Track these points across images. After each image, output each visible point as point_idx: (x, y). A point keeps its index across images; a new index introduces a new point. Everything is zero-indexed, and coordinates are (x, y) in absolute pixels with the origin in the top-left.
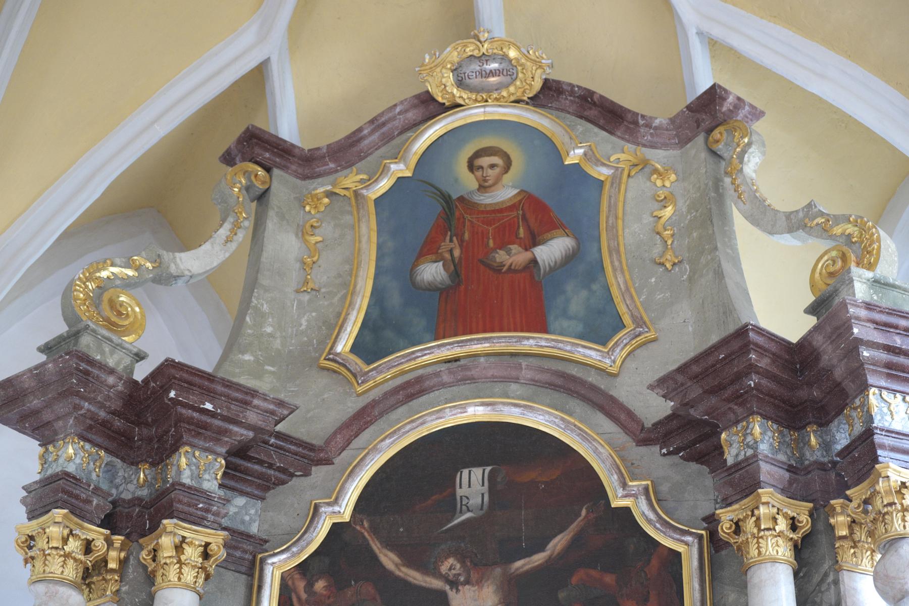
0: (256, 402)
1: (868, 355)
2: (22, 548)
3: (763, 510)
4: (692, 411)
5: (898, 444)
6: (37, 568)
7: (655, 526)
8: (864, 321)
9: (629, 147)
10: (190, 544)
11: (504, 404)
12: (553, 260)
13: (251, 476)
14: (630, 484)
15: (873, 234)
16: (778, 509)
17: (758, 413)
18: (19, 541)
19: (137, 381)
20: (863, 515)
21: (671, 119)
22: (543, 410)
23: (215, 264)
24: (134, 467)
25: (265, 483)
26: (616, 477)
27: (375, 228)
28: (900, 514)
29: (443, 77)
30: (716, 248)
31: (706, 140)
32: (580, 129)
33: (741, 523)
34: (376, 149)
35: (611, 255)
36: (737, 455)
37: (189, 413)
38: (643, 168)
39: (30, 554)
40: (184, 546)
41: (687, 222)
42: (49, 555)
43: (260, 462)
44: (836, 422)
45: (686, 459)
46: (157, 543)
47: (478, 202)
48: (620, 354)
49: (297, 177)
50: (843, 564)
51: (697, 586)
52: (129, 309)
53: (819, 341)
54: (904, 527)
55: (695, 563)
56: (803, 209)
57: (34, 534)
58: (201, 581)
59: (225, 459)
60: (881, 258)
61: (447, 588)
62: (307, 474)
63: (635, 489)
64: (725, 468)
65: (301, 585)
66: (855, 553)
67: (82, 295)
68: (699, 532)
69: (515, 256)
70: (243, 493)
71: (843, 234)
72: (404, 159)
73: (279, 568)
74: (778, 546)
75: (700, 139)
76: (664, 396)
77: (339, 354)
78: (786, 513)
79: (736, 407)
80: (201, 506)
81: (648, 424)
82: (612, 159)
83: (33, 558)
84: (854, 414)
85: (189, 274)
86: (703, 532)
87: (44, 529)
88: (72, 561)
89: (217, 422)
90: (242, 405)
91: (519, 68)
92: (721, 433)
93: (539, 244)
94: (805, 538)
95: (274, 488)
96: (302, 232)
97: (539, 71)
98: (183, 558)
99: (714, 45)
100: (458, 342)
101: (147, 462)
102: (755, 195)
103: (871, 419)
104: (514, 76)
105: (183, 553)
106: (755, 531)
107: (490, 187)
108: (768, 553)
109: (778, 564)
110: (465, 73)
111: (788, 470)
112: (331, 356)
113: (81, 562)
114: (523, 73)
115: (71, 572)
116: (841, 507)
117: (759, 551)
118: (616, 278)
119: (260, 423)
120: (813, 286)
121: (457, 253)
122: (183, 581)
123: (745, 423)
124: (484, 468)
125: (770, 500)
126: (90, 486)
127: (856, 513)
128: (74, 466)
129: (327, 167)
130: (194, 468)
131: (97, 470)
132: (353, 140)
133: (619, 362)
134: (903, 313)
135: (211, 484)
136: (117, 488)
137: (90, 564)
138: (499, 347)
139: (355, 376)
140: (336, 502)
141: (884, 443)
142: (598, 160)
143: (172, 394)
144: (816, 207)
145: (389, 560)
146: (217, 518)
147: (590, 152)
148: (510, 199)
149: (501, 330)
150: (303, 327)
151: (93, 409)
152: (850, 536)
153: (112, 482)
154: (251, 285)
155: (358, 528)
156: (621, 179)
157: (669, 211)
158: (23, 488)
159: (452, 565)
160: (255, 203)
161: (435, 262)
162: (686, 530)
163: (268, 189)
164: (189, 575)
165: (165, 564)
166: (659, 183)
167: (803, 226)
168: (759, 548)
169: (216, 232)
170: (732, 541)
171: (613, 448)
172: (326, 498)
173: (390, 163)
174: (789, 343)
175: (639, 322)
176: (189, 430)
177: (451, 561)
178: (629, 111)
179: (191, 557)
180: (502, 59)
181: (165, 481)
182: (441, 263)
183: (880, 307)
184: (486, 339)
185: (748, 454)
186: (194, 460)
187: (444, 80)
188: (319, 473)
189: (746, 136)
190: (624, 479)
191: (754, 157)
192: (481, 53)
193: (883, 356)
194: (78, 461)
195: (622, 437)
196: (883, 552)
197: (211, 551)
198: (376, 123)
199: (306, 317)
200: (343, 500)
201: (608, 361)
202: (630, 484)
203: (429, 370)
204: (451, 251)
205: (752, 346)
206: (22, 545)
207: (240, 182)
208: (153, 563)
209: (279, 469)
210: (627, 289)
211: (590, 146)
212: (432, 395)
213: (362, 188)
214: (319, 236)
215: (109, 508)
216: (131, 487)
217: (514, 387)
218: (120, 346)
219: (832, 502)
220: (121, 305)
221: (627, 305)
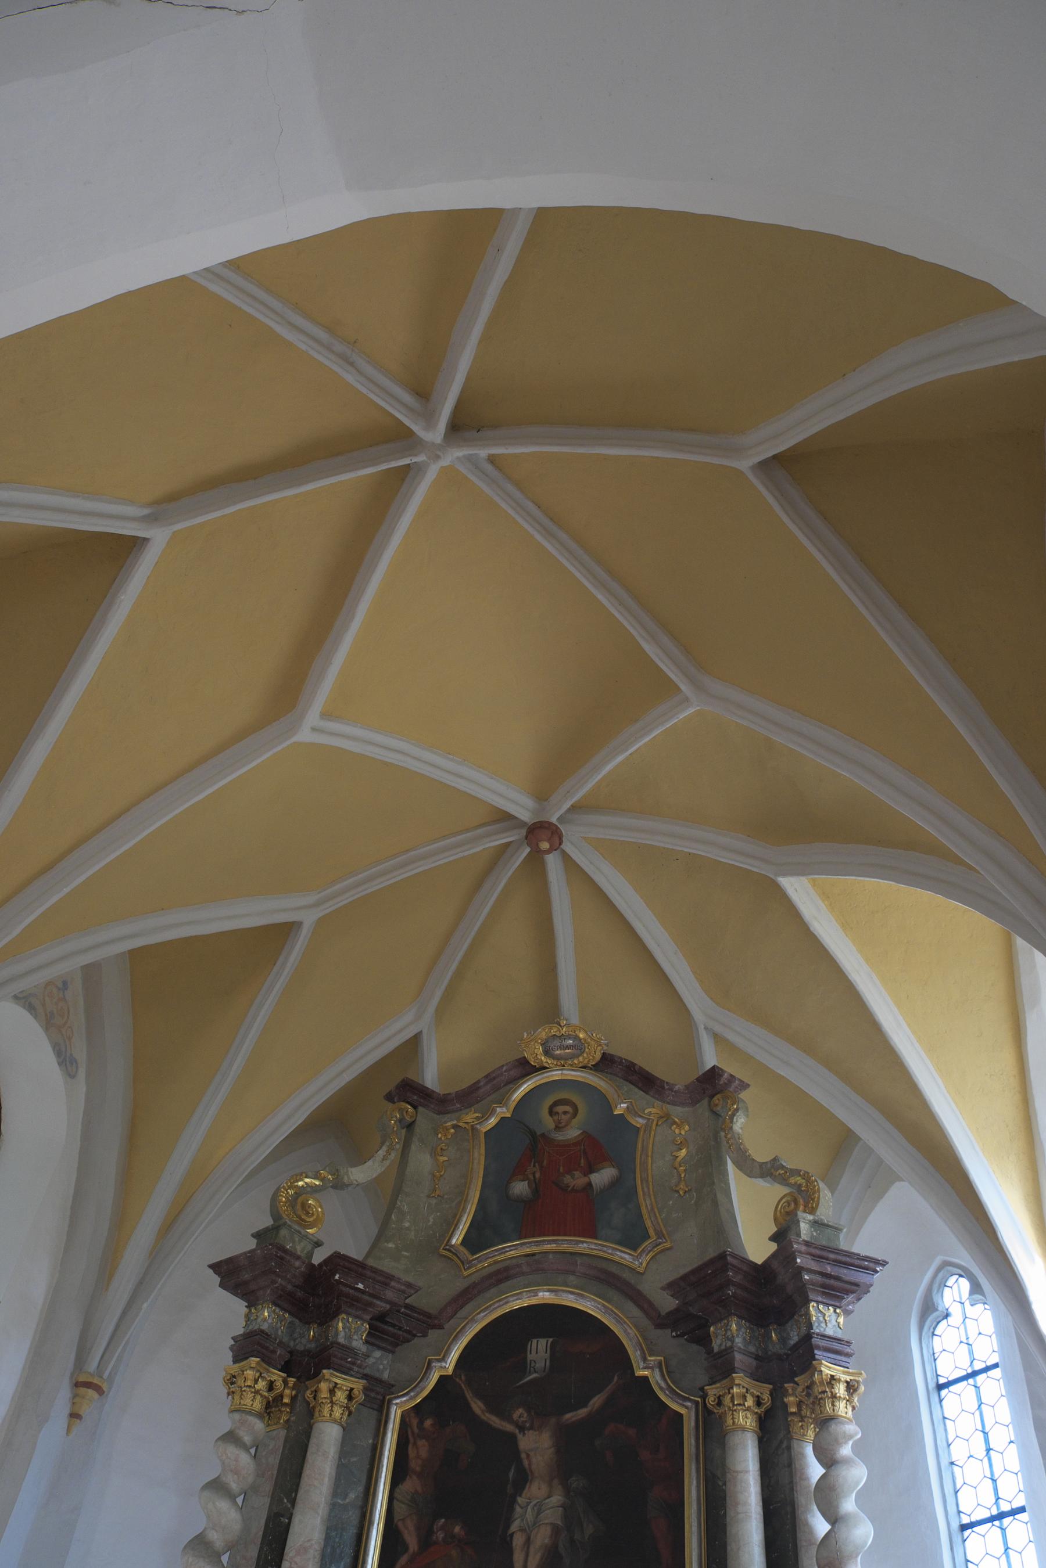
0: (393, 1284)
1: (808, 1278)
2: (227, 1384)
3: (735, 1390)
4: (690, 1309)
5: (829, 1346)
6: (235, 1400)
7: (665, 1393)
8: (804, 1254)
9: (658, 1103)
10: (340, 1389)
11: (564, 1291)
12: (603, 1184)
13: (386, 1335)
14: (649, 1358)
15: (815, 1186)
16: (747, 1389)
17: (735, 1315)
18: (226, 1379)
19: (314, 1265)
20: (806, 1398)
21: (685, 1086)
22: (590, 1298)
23: (374, 1176)
24: (307, 1326)
25: (395, 1341)
26: (639, 1352)
27: (484, 1153)
28: (830, 1400)
29: (535, 1048)
30: (713, 1183)
31: (710, 1102)
32: (625, 1088)
33: (721, 1398)
34: (489, 1095)
35: (642, 1183)
36: (721, 1345)
37: (347, 1290)
38: (666, 1120)
39: (231, 1390)
40: (336, 1390)
41: (695, 1161)
42: (244, 1391)
43: (393, 1326)
44: (790, 1324)
45: (689, 1341)
46: (318, 1386)
47: (555, 1138)
48: (645, 1260)
49: (434, 1113)
50: (793, 1434)
51: (693, 1442)
52: (314, 1210)
53: (775, 1265)
54: (834, 1410)
55: (693, 1424)
56: (770, 1161)
57: (236, 1374)
58: (345, 1417)
59: (369, 1324)
60: (820, 1205)
61: (517, 1431)
62: (425, 1335)
63: (652, 1363)
64: (712, 1355)
65: (415, 1422)
66: (802, 1425)
67: (284, 1199)
68: (697, 1399)
69: (576, 1180)
70: (379, 1348)
71: (796, 1183)
72: (506, 1105)
73: (400, 1407)
74: (746, 1417)
75: (705, 1102)
76: (672, 1296)
77: (453, 1245)
78: (753, 1392)
79: (720, 1308)
80: (349, 1360)
81: (663, 1313)
82: (646, 1112)
83: (233, 1392)
84: (801, 1320)
85: (357, 1183)
86: (699, 1400)
87: (243, 1371)
88: (259, 1396)
89: (366, 1297)
90: (382, 1285)
91: (586, 1045)
92: (710, 1327)
93: (594, 1172)
94: (767, 1412)
95: (401, 1345)
96: (434, 1154)
97: (599, 1048)
98: (334, 1399)
99: (717, 1038)
100: (535, 1242)
101: (316, 1323)
102: (740, 1148)
103: (810, 1326)
104: (582, 1051)
105: (334, 1396)
106: (731, 1405)
107: (563, 1127)
108: (739, 1423)
109: (746, 1432)
110: (550, 1047)
111: (755, 1359)
112: (448, 1247)
113: (265, 1397)
114: (588, 1048)
115: (258, 1405)
116: (792, 1389)
117: (733, 1421)
118: (645, 1201)
119: (394, 1299)
120: (776, 1220)
121: (538, 1175)
122: (333, 1416)
123: (726, 1321)
124: (548, 1339)
125: (741, 1382)
126: (276, 1340)
127: (801, 1396)
128: (267, 1325)
129: (455, 1107)
130: (347, 1330)
131: (282, 1328)
132: (474, 1088)
133: (644, 1264)
134: (831, 1249)
135: (358, 1343)
136: (295, 1340)
137: (271, 1399)
138: (565, 1247)
139: (463, 1263)
140: (443, 1359)
141: (818, 1344)
142: (637, 1113)
143: (337, 1277)
144: (779, 1161)
145: (477, 1406)
146: (360, 1369)
147: (631, 1107)
148: (576, 1137)
149: (565, 1235)
150: (431, 1223)
151: (283, 1283)
152: (798, 1413)
153: (291, 1336)
154: (398, 1191)
155: (457, 1380)
156: (651, 1127)
157: (683, 1152)
158: (232, 1338)
159: (521, 1414)
160: (404, 1131)
161: (523, 1181)
162: (686, 1397)
163: (415, 1120)
164: (337, 1412)
165: (322, 1403)
166: (677, 1131)
167: (771, 1175)
168: (733, 1418)
169: (377, 1152)
170: (716, 1411)
171: (638, 1330)
172: (437, 1356)
173: (496, 1107)
174: (756, 1264)
175: (660, 1234)
176: (347, 1302)
177: (521, 1410)
178: (659, 1079)
179: (340, 1398)
180: (575, 1038)
181: (327, 1338)
182: (527, 1182)
183: (815, 1244)
184: (554, 1241)
185: (727, 1345)
186: (348, 1324)
187: (536, 1050)
188: (433, 1334)
189: (735, 1104)
190: (645, 1354)
191: (740, 1118)
192: (561, 1034)
193: (818, 1278)
194: (270, 1321)
195: (645, 1322)
196: (820, 1427)
197: (354, 1394)
198: (489, 1078)
199: (433, 1216)
200: (449, 1358)
201: (637, 1263)
202: (649, 1358)
203: (514, 1261)
204: (534, 1174)
205: (729, 1266)
206: (227, 1382)
207: (396, 1117)
208: (313, 1400)
209: (406, 1331)
210: (652, 1209)
211: (631, 1102)
212: (515, 1280)
213: (476, 1124)
214: (446, 1156)
215: (287, 1357)
216: (304, 1341)
217: (572, 1278)
218: (306, 1237)
219: (786, 1385)
220: (309, 1207)
221: (652, 1221)
